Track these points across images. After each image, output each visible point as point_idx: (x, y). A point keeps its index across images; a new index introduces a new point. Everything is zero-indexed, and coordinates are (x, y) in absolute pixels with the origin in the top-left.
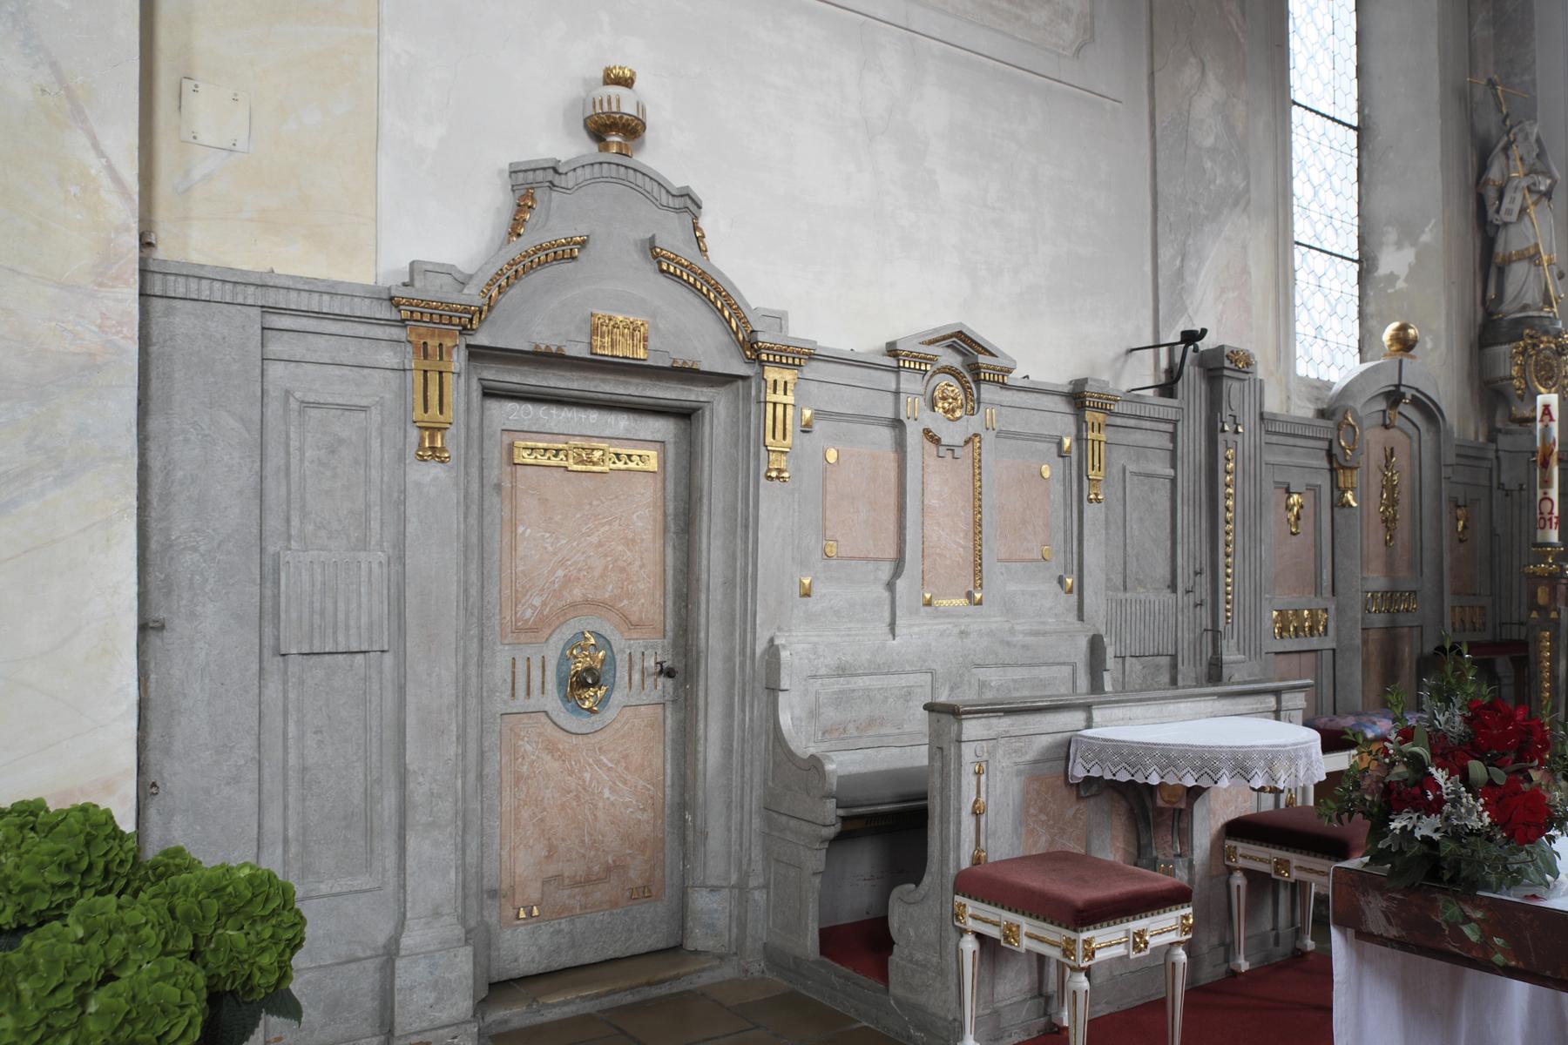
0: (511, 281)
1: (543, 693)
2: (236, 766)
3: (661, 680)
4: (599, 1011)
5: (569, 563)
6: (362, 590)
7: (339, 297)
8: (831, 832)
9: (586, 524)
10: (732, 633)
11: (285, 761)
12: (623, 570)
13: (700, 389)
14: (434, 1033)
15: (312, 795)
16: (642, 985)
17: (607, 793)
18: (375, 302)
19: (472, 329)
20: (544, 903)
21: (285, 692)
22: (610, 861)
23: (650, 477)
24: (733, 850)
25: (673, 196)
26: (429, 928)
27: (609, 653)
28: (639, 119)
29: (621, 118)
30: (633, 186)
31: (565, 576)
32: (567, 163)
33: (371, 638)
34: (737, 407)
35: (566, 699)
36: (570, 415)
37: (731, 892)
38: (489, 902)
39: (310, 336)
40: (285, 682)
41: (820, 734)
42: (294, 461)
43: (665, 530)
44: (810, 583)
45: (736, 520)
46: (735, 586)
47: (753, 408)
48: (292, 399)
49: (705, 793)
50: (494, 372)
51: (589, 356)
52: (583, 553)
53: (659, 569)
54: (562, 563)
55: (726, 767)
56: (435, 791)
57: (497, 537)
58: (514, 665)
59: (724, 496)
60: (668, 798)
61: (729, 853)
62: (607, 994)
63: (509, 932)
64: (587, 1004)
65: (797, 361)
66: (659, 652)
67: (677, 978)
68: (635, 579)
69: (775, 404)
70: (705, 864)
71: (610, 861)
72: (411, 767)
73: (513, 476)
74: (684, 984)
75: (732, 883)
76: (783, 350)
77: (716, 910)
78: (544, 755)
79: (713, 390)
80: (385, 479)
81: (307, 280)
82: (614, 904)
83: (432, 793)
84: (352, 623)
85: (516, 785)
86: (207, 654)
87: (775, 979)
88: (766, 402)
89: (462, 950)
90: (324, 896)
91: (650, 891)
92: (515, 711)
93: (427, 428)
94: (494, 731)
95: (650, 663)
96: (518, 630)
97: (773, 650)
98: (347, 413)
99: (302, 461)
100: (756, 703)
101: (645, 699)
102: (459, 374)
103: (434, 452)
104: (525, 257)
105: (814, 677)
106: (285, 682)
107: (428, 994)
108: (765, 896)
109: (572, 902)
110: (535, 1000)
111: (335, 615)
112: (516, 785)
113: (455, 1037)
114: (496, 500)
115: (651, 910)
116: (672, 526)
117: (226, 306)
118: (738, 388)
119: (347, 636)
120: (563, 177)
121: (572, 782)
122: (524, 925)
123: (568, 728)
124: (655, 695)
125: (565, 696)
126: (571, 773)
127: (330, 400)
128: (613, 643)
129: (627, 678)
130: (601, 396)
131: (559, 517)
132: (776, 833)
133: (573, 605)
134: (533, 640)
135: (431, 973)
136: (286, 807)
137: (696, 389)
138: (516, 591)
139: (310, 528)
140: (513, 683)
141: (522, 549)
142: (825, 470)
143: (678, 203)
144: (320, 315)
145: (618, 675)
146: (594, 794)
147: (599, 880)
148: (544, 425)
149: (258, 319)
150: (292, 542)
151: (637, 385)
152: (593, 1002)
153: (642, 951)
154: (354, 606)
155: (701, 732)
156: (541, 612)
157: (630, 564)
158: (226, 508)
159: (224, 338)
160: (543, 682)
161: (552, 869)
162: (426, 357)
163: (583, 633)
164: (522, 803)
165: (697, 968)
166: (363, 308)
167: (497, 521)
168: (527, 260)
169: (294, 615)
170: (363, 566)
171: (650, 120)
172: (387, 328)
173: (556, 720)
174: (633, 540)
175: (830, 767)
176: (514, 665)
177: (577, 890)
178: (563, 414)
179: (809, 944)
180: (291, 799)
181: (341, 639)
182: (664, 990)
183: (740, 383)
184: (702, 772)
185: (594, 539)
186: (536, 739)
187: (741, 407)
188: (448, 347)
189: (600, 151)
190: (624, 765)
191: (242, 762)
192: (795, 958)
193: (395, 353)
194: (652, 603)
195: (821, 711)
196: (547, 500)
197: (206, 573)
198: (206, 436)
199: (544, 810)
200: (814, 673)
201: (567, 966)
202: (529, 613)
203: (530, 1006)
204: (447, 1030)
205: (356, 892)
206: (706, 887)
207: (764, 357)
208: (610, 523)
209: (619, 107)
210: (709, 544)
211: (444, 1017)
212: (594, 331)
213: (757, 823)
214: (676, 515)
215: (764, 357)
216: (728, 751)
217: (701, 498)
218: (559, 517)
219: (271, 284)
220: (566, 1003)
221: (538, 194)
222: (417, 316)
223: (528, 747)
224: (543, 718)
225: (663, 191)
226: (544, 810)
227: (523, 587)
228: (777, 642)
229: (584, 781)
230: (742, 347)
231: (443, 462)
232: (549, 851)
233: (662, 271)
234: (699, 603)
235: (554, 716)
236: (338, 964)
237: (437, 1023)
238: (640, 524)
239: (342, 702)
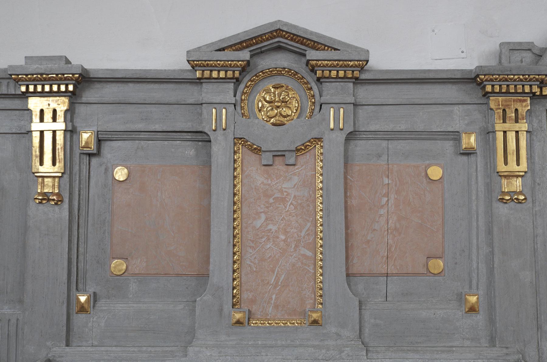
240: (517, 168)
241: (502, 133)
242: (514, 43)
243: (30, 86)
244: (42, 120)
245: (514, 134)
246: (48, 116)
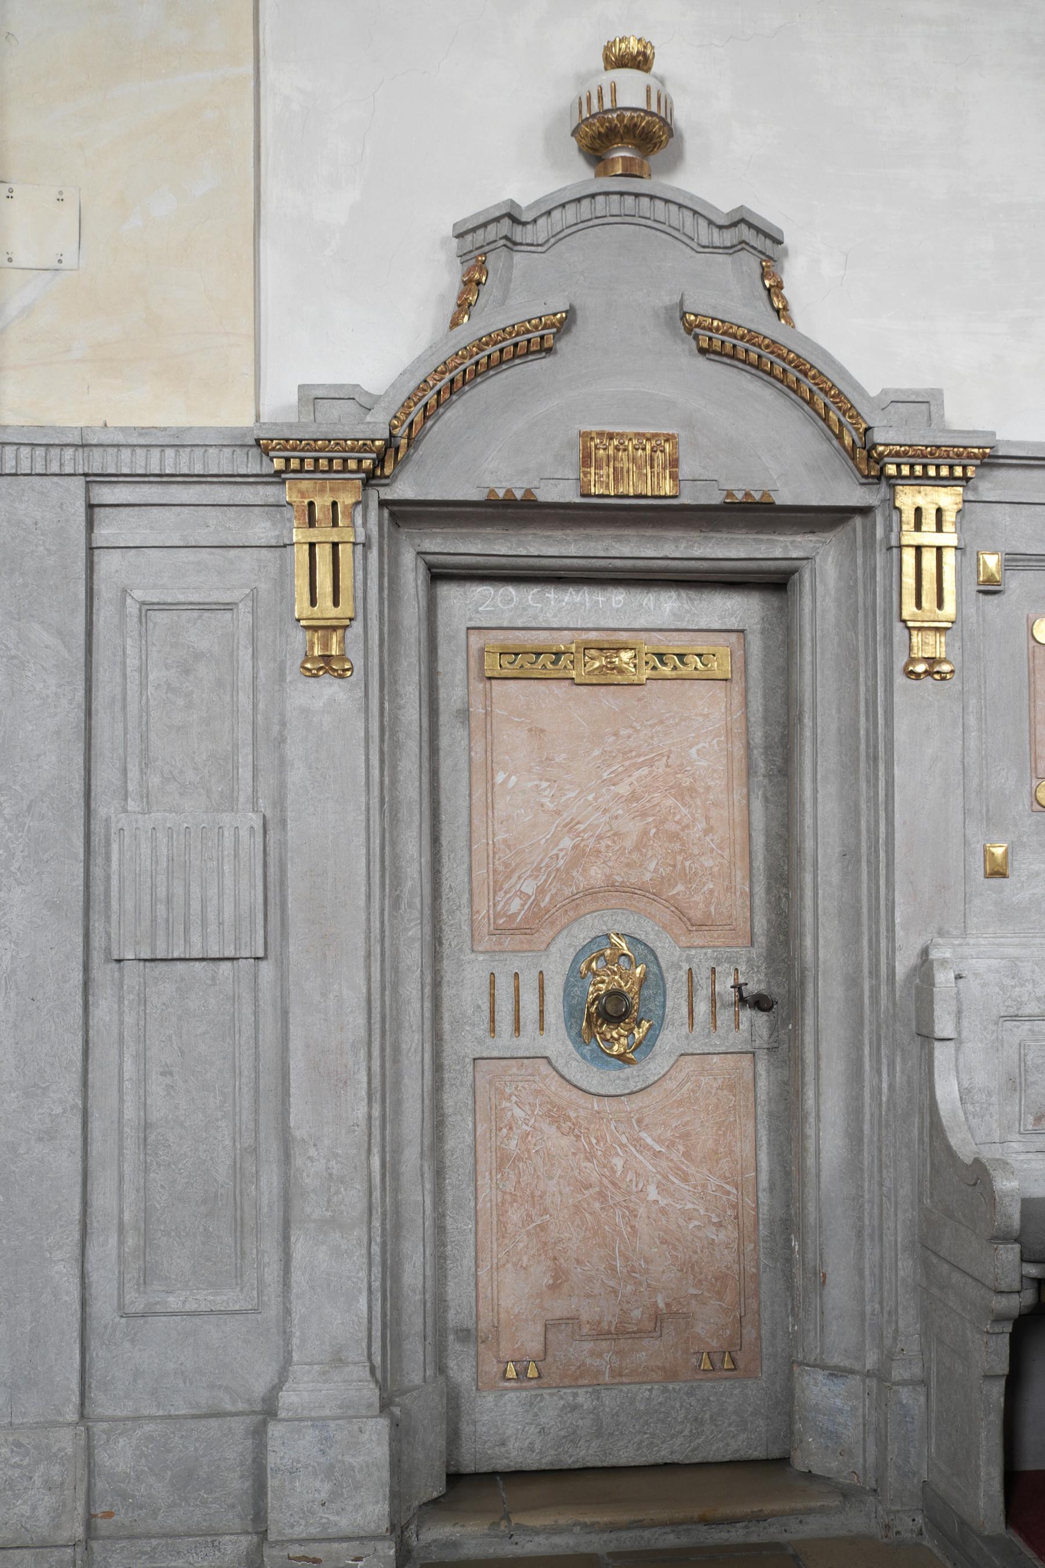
0: (445, 396)
1: (542, 1029)
2: (50, 1115)
3: (747, 1015)
4: (610, 1554)
5: (582, 827)
6: (226, 867)
7: (188, 450)
8: (1014, 1304)
9: (609, 766)
10: (857, 940)
11: (121, 1112)
12: (674, 837)
13: (791, 538)
14: (325, 1546)
15: (159, 1165)
16: (692, 1521)
17: (653, 1193)
18: (238, 450)
19: (384, 476)
20: (549, 1359)
21: (121, 1013)
22: (661, 1305)
23: (719, 688)
24: (868, 1309)
25: (721, 227)
26: (326, 1381)
27: (654, 969)
28: (652, 114)
29: (621, 118)
30: (649, 223)
31: (575, 847)
32: (530, 207)
33: (237, 940)
34: (854, 561)
35: (579, 1040)
36: (578, 598)
37: (864, 1382)
38: (458, 1347)
39: (155, 510)
40: (121, 1000)
41: (1031, 1119)
42: (133, 688)
43: (750, 770)
44: (1006, 853)
45: (857, 749)
46: (859, 861)
47: (880, 559)
48: (129, 601)
49: (819, 1210)
50: (439, 540)
51: (579, 500)
52: (605, 811)
53: (740, 834)
54: (570, 827)
55: (853, 1167)
56: (335, 1172)
57: (463, 790)
58: (492, 983)
59: (839, 711)
60: (764, 1209)
61: (862, 1314)
62: (630, 1526)
63: (491, 1398)
64: (594, 1538)
65: (958, 472)
66: (742, 968)
67: (759, 1518)
68: (696, 851)
69: (918, 549)
70: (822, 1327)
71: (661, 1305)
72: (298, 1134)
73: (488, 696)
74: (772, 1530)
75: (868, 1367)
76: (934, 453)
77: (841, 1411)
78: (545, 1127)
79: (813, 538)
80: (261, 706)
81: (143, 431)
82: (671, 1375)
83: (330, 1175)
84: (211, 916)
85: (500, 1168)
86: (13, 958)
87: (935, 1551)
88: (900, 547)
89: (371, 1422)
90: (173, 1314)
91: (733, 1361)
92: (495, 1054)
93: (315, 629)
94: (462, 1085)
95: (725, 986)
96: (498, 931)
97: (924, 967)
98: (206, 614)
99: (143, 686)
100: (898, 1060)
101: (717, 1043)
102: (366, 546)
103: (328, 663)
104: (463, 357)
105: (1014, 1017)
106: (121, 1000)
107: (318, 1484)
108: (922, 1399)
109: (597, 1362)
110: (506, 1517)
111: (187, 904)
112: (500, 1168)
113: (358, 1559)
114: (461, 733)
115: (736, 1392)
116: (762, 764)
117: (38, 478)
118: (854, 530)
119: (204, 937)
120: (529, 227)
121: (592, 1171)
122: (513, 1389)
123: (585, 1086)
124: (737, 1039)
125: (580, 1034)
126: (590, 1157)
127: (181, 598)
128: (658, 952)
129: (685, 1010)
130: (619, 563)
131: (564, 755)
132: (934, 1290)
133: (591, 893)
134: (526, 947)
135: (323, 1452)
136: (121, 1180)
137: (781, 538)
138: (495, 871)
139: (155, 780)
140: (492, 1012)
141: (502, 806)
142: (1032, 656)
143: (729, 238)
144: (163, 479)
145: (669, 1004)
146: (630, 1193)
147: (639, 1333)
148: (535, 617)
149: (81, 492)
150: (129, 800)
151: (676, 540)
152: (605, 1536)
153: (719, 1458)
154: (213, 891)
155: (810, 1103)
156: (536, 903)
157: (687, 827)
158: (39, 756)
159: (36, 524)
160: (542, 1012)
161: (560, 1307)
162: (312, 523)
163: (608, 936)
164: (508, 1197)
165: (799, 1505)
166: (220, 462)
167: (463, 764)
168: (468, 363)
169: (129, 905)
170: (226, 833)
171: (681, 118)
172: (260, 488)
173: (565, 1071)
174: (691, 790)
175: (1005, 1184)
176: (492, 983)
177: (604, 1344)
178: (566, 599)
179: (981, 1504)
180: (127, 1169)
181: (196, 938)
182: (735, 1535)
183: (858, 521)
184: (813, 1171)
185: (624, 789)
186: (531, 1100)
187: (860, 561)
188: (345, 506)
189: (597, 175)
190: (682, 1149)
191: (59, 1111)
192: (963, 1523)
193: (274, 524)
194: (728, 889)
195: (1031, 1079)
196: (542, 731)
197: (11, 846)
198: (13, 657)
199: (546, 1211)
200: (1012, 1011)
201: (589, 1465)
202: (515, 905)
203: (495, 1525)
204: (345, 1545)
205: (221, 1312)
206: (824, 1368)
207: (892, 470)
208: (650, 763)
209: (614, 100)
210: (815, 791)
211: (344, 1523)
212: (586, 459)
213: (906, 1267)
214: (767, 748)
215: (892, 470)
216: (855, 1138)
217: (800, 719)
218: (564, 755)
219: (95, 442)
220: (557, 1530)
221: (492, 261)
222: (294, 464)
223: (518, 1112)
224: (543, 1068)
225: (703, 223)
226: (546, 1211)
227: (506, 865)
228: (935, 954)
229: (613, 1171)
230: (853, 459)
231: (341, 677)
232: (555, 1278)
233: (702, 351)
234: (802, 889)
235: (560, 1064)
236: (194, 1417)
237: (332, 1531)
238: (704, 763)
239: (199, 1031)
240: (334, 612)
241: (307, 547)
242: (896, 391)
243: (903, 467)
244: (918, 527)
245: (328, 548)
246: (929, 521)
